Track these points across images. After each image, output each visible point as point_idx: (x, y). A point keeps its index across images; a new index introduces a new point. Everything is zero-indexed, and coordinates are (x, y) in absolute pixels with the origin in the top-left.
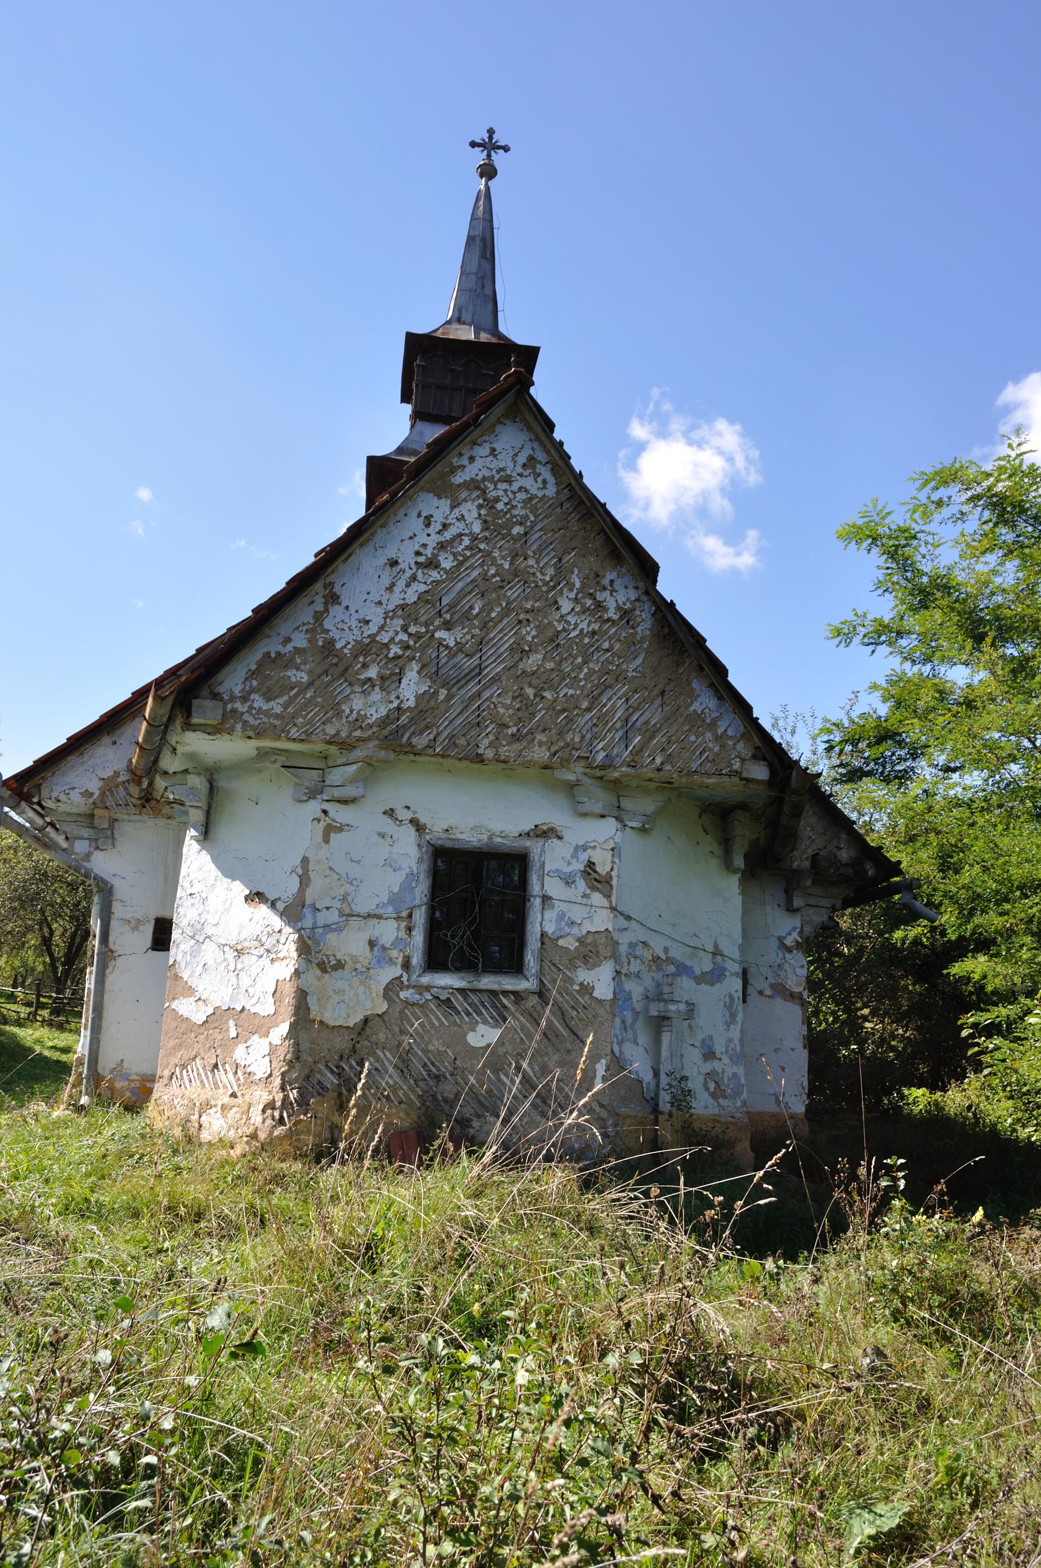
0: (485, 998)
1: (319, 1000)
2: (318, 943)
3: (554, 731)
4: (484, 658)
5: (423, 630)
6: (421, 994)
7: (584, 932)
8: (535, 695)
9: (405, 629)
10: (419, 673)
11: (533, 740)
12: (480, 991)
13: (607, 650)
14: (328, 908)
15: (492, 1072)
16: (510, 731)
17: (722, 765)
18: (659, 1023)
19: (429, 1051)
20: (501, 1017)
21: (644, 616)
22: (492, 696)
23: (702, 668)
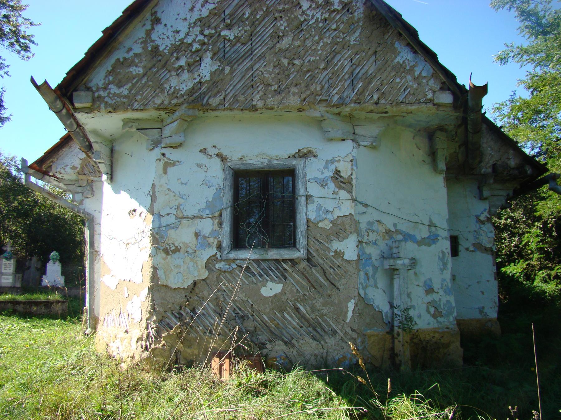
0: (272, 264)
1: (165, 272)
2: (162, 237)
3: (303, 85)
4: (253, 44)
5: (213, 31)
6: (229, 265)
7: (335, 217)
8: (289, 64)
9: (202, 33)
10: (212, 58)
11: (289, 92)
12: (268, 260)
13: (335, 30)
14: (168, 215)
15: (279, 312)
16: (273, 88)
17: (420, 97)
18: (392, 272)
19: (236, 301)
20: (283, 277)
21: (358, 5)
22: (260, 67)
23: (400, 35)
